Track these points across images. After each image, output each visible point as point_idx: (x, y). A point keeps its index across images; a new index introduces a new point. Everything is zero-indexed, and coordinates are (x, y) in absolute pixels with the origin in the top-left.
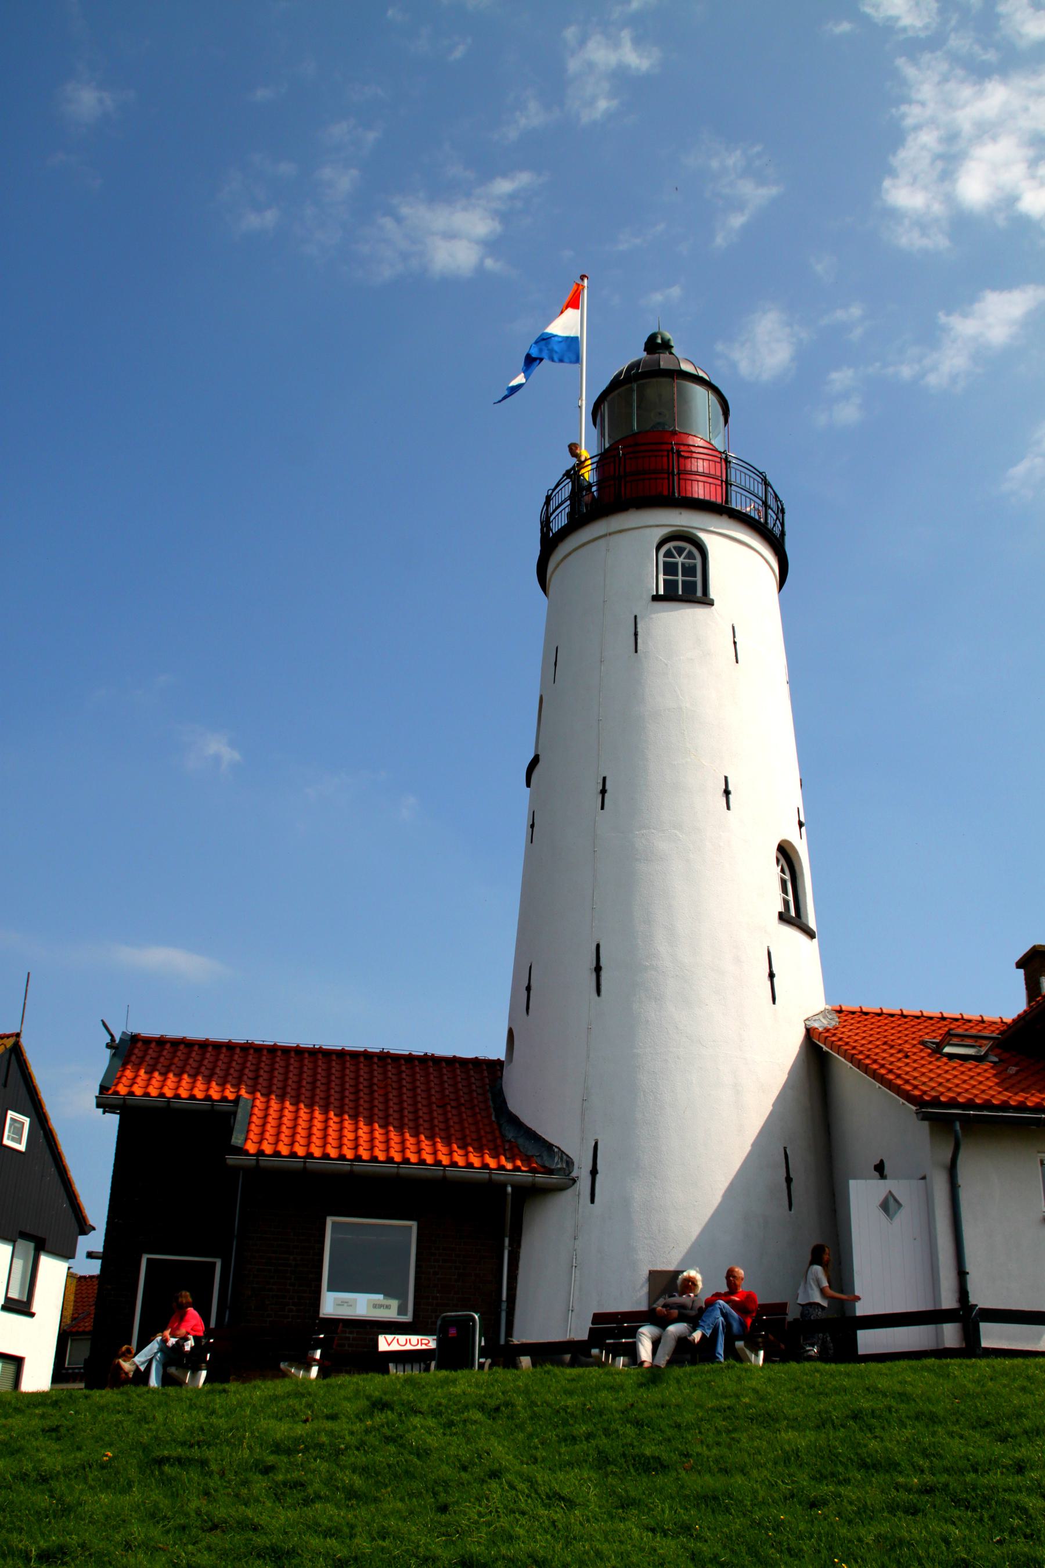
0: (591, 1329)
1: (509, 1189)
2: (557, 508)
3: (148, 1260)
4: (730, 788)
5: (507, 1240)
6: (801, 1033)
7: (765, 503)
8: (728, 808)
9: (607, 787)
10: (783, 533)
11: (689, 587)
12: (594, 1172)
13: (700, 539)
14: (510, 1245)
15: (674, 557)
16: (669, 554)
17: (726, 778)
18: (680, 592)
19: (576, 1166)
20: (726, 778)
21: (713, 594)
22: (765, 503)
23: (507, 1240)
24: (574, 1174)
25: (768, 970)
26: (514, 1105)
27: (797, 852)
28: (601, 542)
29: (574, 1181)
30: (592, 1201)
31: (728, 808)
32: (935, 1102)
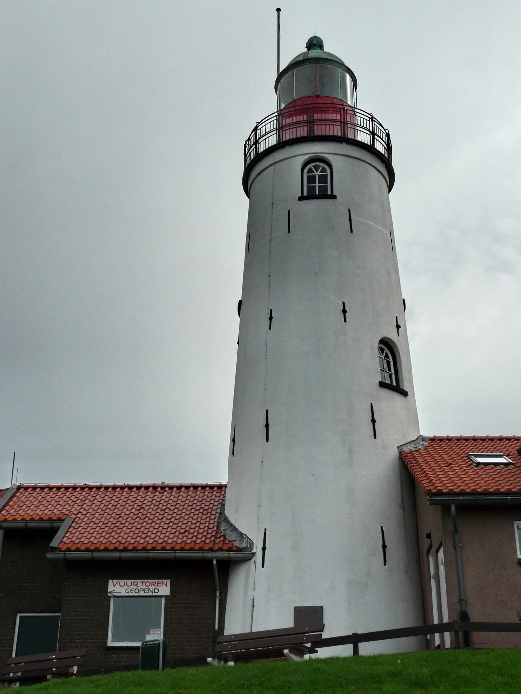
0: (322, 631)
1: (215, 562)
3: (20, 616)
4: (346, 309)
5: (218, 593)
6: (396, 452)
10: (389, 148)
11: (323, 189)
12: (264, 549)
14: (220, 596)
15: (314, 173)
16: (310, 171)
18: (317, 193)
19: (255, 546)
22: (373, 134)
23: (218, 593)
24: (254, 551)
25: (371, 418)
26: (228, 512)
27: (395, 344)
29: (254, 554)
30: (263, 566)
31: (345, 321)
32: (440, 493)
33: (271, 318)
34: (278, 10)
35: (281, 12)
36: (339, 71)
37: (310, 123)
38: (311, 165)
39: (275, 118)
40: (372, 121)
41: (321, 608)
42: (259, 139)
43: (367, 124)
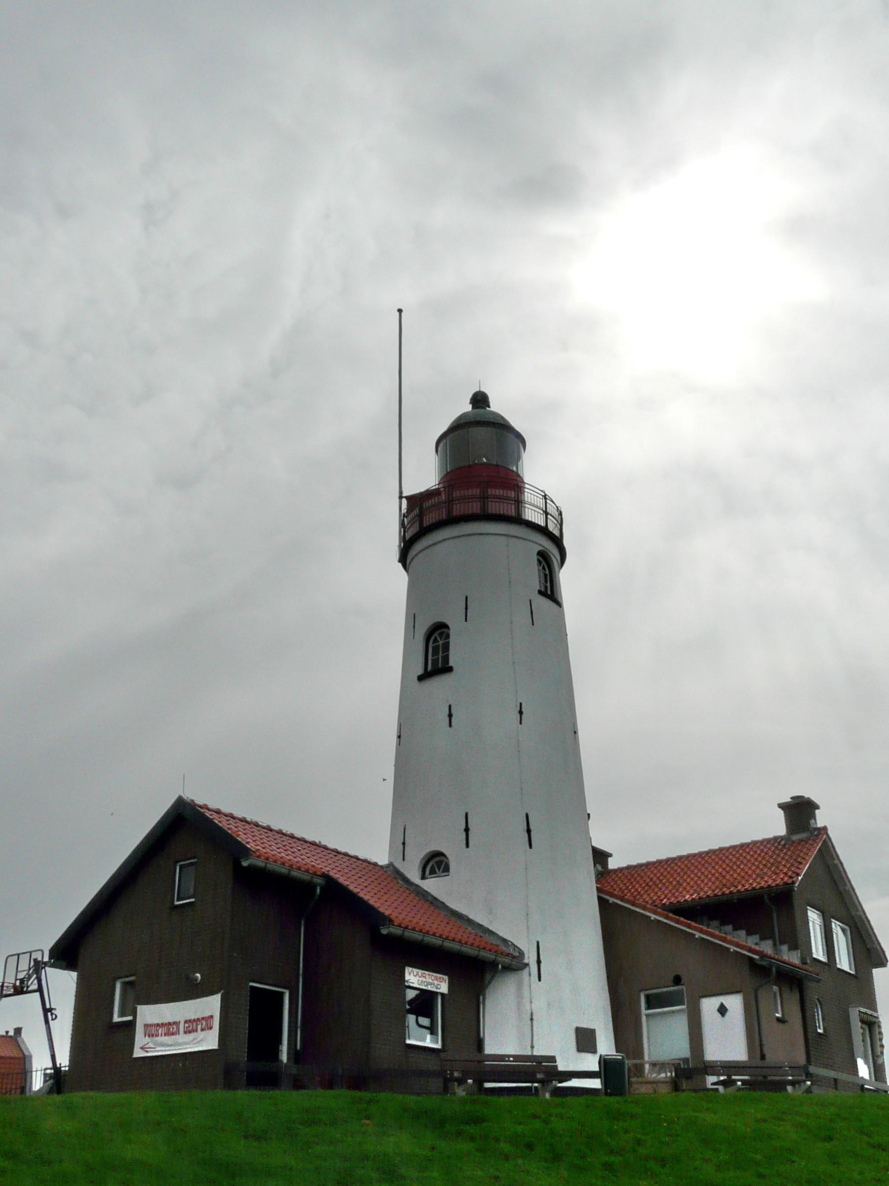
12: (539, 962)
24: (526, 961)
33: (450, 716)
34: (400, 311)
35: (403, 314)
36: (511, 436)
37: (484, 498)
38: (436, 634)
40: (546, 499)
41: (593, 1032)
43: (541, 502)
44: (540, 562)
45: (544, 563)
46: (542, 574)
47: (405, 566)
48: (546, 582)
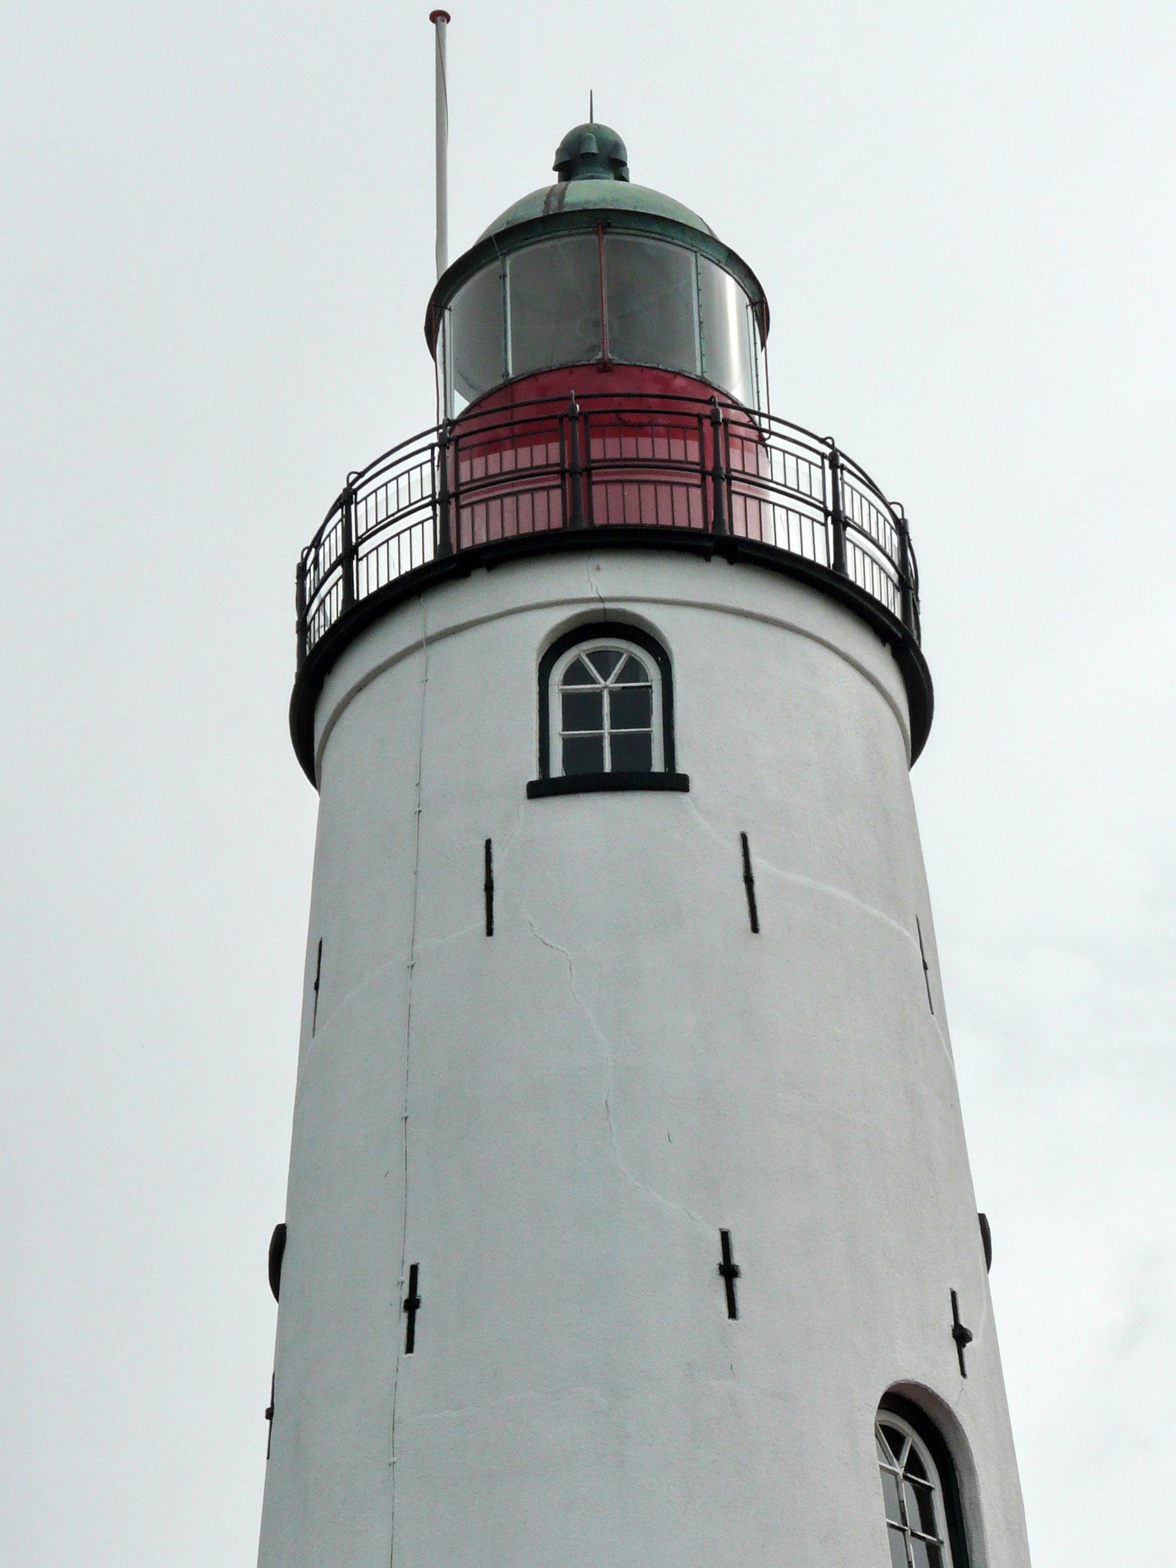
2: (317, 591)
4: (737, 1259)
7: (839, 521)
8: (733, 1313)
9: (421, 1292)
10: (907, 585)
11: (633, 749)
13: (640, 619)
15: (593, 681)
16: (576, 673)
17: (725, 1236)
18: (608, 768)
20: (725, 1236)
21: (683, 766)
22: (839, 521)
28: (414, 663)
31: (733, 1313)
33: (412, 1305)
38: (579, 652)
39: (427, 455)
40: (834, 466)
42: (362, 540)
43: (815, 482)
44: (892, 1439)
45: (913, 1439)
46: (908, 1494)
47: (277, 1296)
48: (928, 1524)
